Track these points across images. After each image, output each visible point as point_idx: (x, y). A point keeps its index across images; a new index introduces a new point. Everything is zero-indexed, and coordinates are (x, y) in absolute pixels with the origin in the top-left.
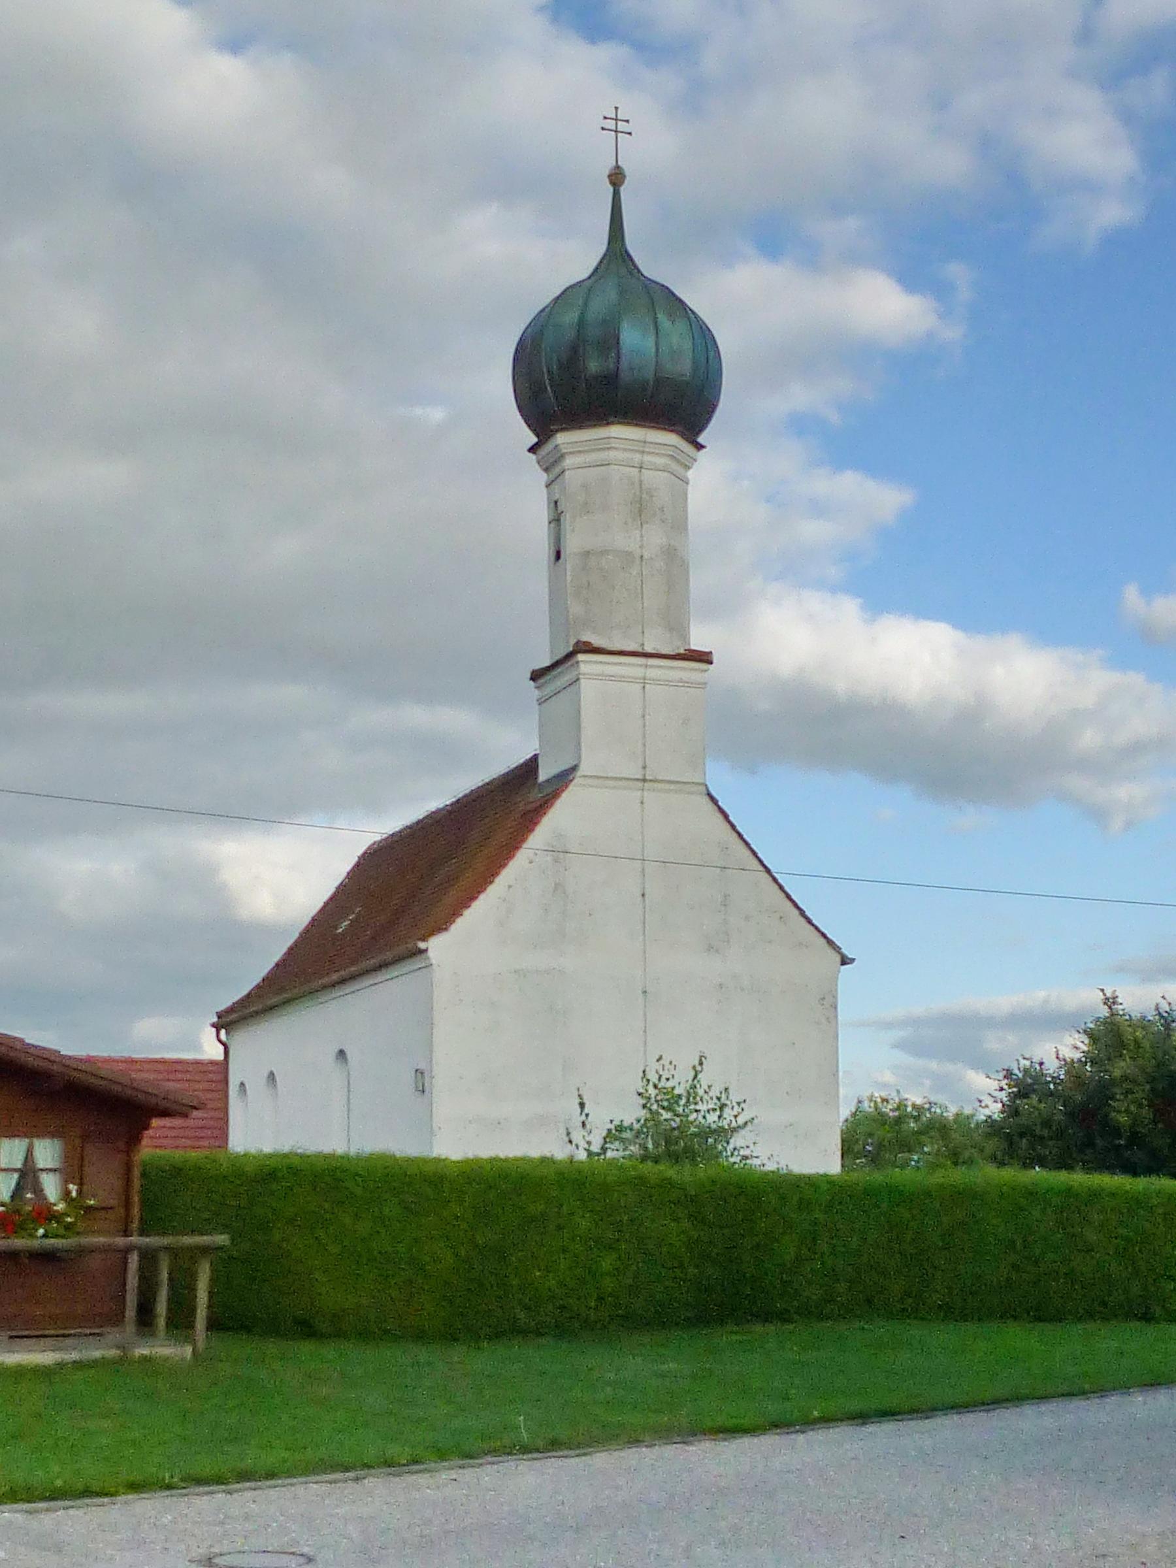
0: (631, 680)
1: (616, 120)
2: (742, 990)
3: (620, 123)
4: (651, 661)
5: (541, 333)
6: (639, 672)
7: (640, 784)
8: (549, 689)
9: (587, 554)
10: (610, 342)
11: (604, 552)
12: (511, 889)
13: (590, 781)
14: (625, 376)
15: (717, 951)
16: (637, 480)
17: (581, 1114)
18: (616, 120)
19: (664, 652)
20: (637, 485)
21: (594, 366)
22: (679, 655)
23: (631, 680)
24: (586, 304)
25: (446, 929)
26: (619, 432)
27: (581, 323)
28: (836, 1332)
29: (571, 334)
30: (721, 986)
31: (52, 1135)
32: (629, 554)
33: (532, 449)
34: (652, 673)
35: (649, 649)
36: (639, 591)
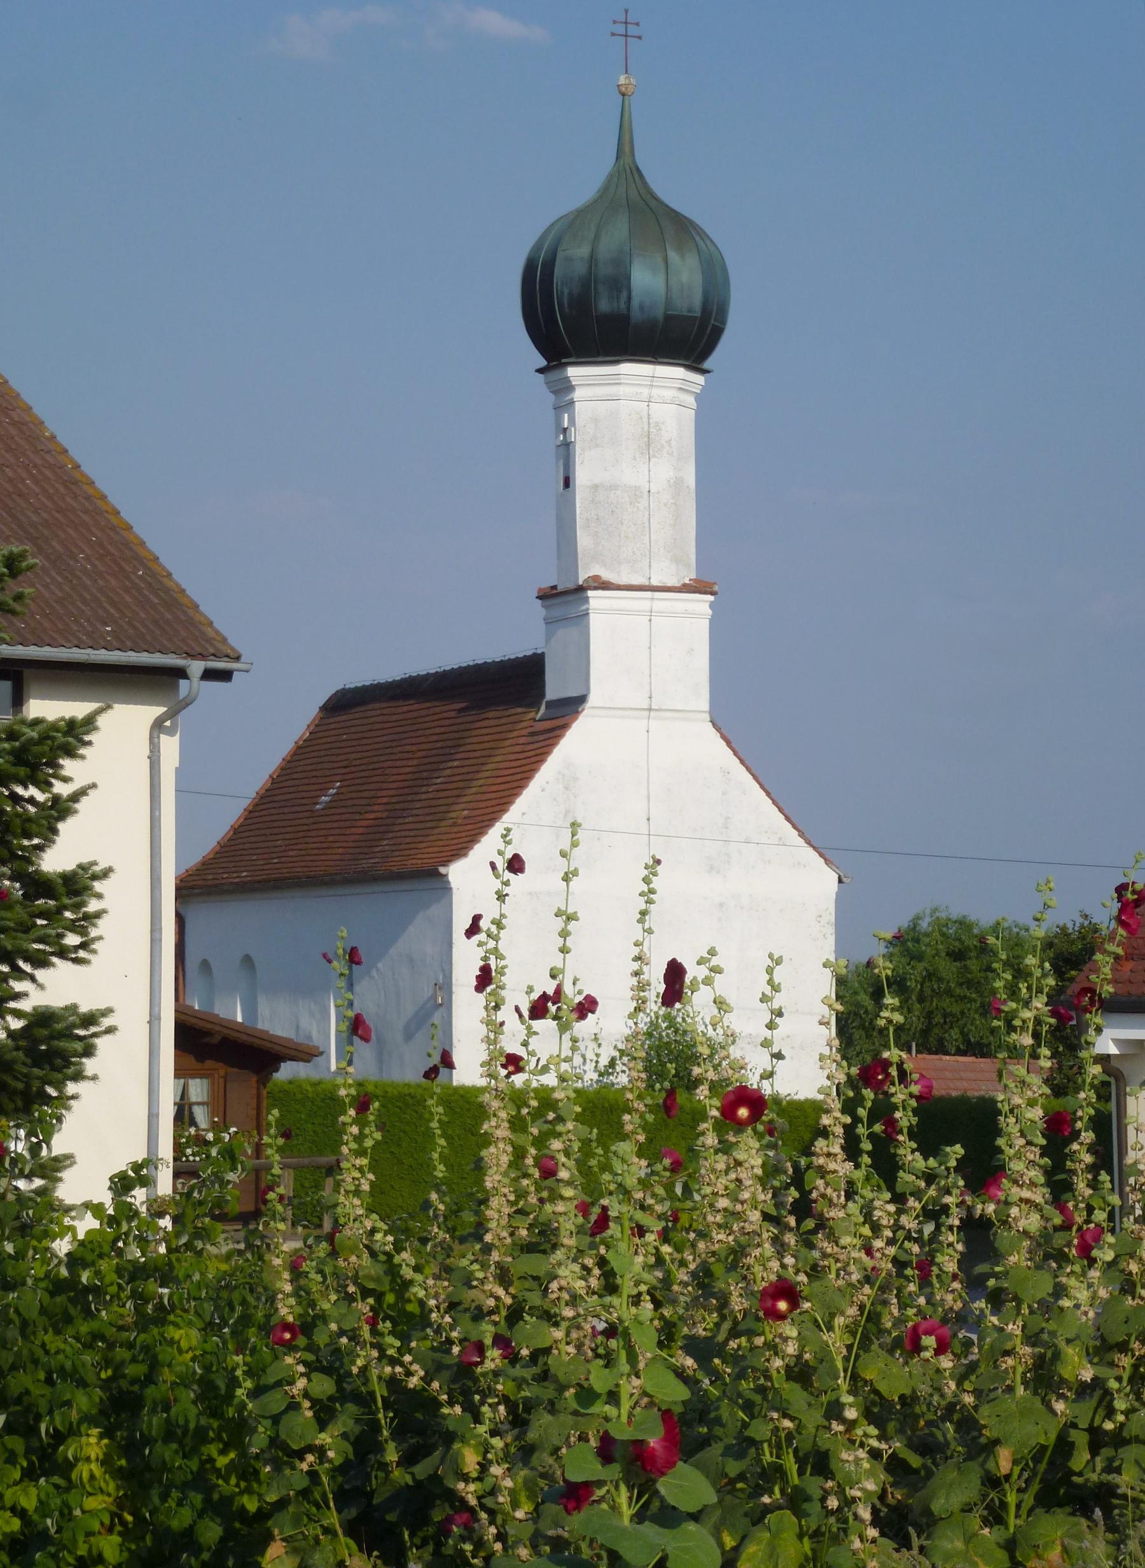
0: (638, 613)
1: (626, 36)
2: (742, 908)
3: (629, 26)
4: (657, 595)
5: (550, 264)
6: (646, 605)
7: (646, 713)
8: (558, 612)
9: (595, 487)
10: (620, 283)
11: (613, 487)
12: (575, 883)
13: (598, 712)
14: (636, 315)
15: (718, 872)
16: (645, 413)
17: (13, 612)
18: (626, 23)
19: (669, 584)
20: (645, 420)
21: (604, 305)
22: (684, 585)
23: (638, 613)
24: (597, 237)
25: (465, 855)
26: (628, 369)
27: (592, 259)
28: (116, 1296)
29: (580, 269)
30: (721, 905)
31: (201, 1076)
32: (637, 488)
33: (540, 371)
34: (658, 606)
35: (655, 582)
36: (647, 525)
